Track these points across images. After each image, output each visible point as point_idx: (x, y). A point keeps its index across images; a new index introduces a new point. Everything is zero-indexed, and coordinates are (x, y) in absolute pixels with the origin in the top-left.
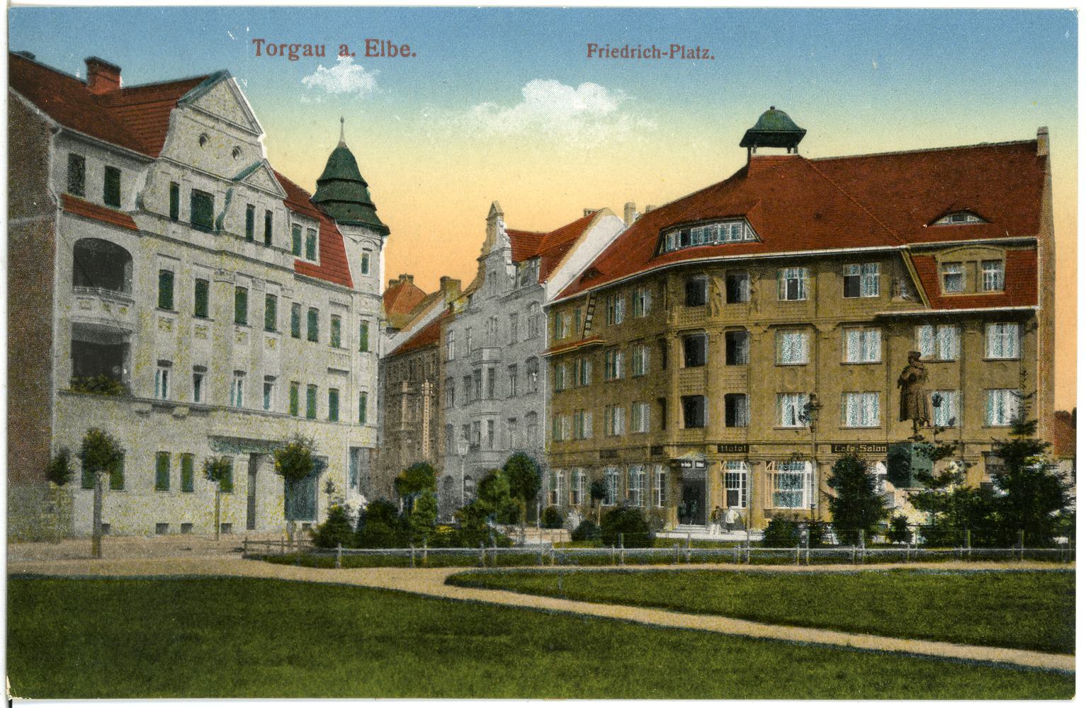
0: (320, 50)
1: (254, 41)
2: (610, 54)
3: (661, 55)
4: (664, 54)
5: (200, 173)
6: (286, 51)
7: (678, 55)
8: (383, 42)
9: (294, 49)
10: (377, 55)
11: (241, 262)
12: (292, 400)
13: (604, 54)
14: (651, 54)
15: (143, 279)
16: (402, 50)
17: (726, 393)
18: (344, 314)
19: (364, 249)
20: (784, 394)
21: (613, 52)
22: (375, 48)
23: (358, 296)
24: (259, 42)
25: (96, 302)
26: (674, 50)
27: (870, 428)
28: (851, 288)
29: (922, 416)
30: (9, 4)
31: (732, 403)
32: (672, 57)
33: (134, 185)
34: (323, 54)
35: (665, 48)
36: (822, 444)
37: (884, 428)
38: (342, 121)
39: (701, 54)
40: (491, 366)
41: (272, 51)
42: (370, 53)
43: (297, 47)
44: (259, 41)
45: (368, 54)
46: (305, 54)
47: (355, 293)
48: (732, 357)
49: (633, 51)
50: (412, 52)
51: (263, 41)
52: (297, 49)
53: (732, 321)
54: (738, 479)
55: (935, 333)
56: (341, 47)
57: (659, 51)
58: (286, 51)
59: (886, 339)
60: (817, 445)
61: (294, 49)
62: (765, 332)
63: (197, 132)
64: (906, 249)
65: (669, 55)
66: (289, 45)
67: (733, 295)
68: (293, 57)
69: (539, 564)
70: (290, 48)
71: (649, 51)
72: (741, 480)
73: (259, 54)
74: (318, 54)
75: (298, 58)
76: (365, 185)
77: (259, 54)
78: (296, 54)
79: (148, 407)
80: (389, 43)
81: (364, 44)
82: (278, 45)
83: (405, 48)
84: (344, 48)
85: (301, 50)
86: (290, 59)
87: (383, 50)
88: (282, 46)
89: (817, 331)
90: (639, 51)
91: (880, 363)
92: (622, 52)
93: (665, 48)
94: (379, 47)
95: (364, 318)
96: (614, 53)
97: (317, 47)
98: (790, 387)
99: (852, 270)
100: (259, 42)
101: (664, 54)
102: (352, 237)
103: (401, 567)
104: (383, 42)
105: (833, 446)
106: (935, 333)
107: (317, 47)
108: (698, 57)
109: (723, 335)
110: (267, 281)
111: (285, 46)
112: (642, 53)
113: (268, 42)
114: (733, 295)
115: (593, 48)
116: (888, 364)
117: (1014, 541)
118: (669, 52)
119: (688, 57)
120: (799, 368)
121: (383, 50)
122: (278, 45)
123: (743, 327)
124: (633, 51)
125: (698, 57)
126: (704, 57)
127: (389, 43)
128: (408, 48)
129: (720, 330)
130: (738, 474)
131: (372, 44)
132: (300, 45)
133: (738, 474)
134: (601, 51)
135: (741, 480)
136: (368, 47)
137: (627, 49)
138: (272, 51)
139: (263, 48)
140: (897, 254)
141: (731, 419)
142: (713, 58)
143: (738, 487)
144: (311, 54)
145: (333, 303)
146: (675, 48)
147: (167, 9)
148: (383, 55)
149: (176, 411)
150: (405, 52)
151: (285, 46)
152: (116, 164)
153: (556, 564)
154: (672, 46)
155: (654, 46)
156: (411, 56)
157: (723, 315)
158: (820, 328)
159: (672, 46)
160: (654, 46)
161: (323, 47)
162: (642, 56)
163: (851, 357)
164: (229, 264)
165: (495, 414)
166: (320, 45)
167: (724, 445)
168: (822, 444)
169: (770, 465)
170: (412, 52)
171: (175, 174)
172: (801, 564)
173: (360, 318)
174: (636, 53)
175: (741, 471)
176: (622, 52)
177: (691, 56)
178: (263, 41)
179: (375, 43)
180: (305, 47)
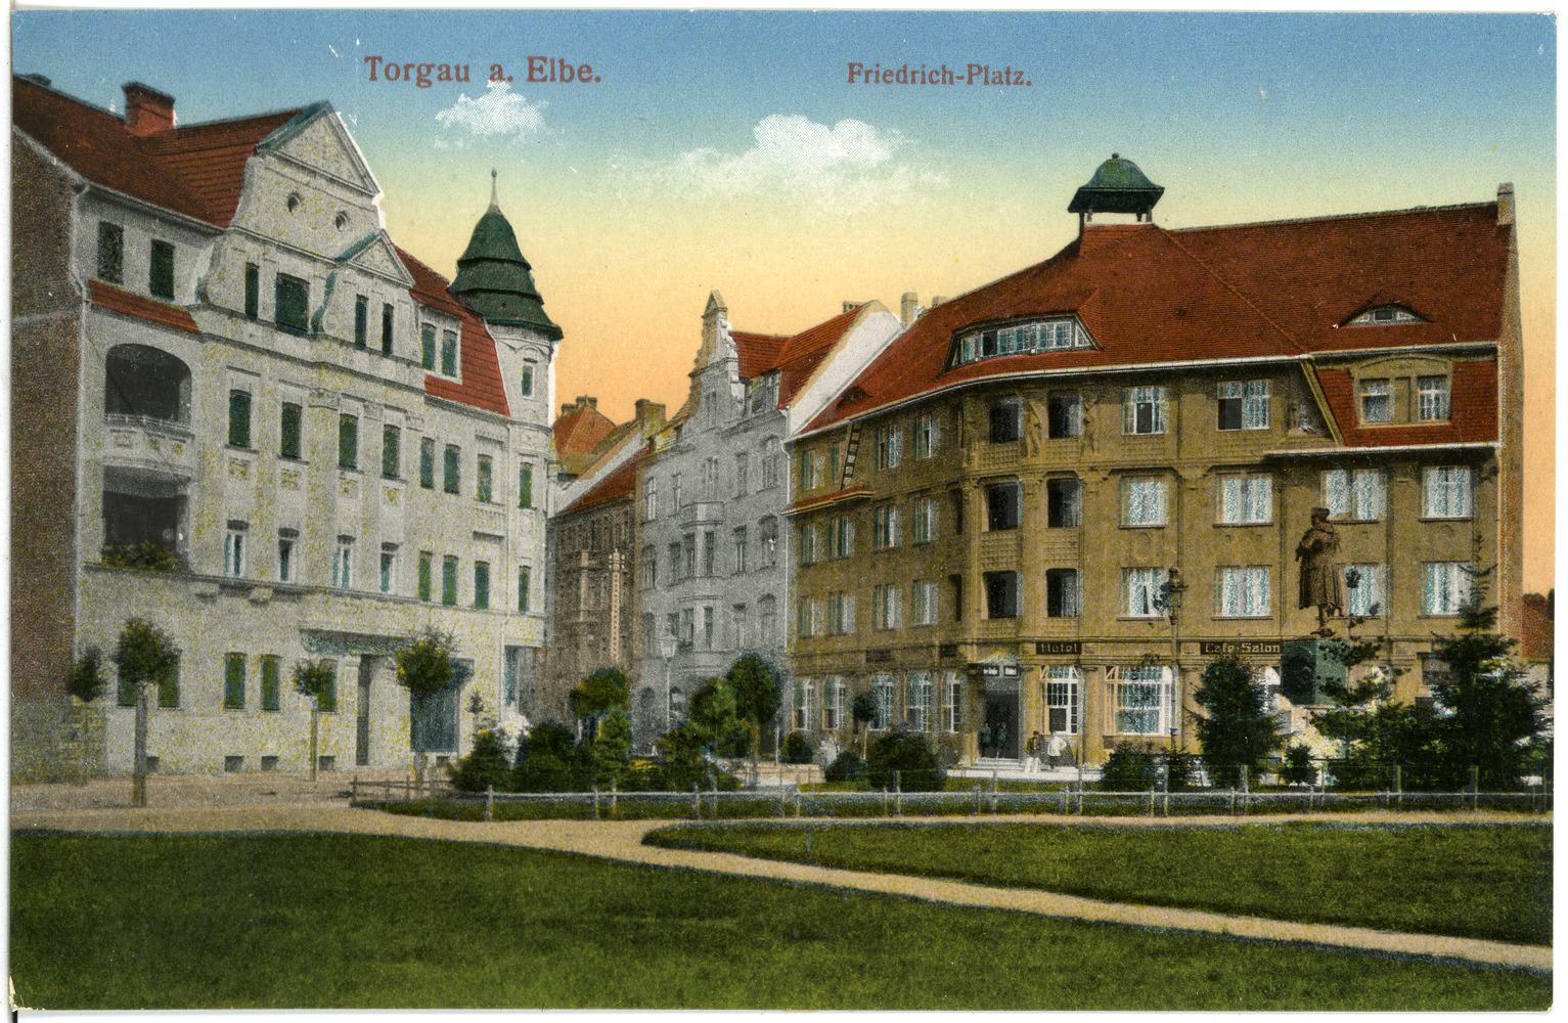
0: (462, 72)
1: (367, 59)
2: (880, 79)
3: (955, 80)
4: (959, 78)
5: (289, 250)
6: (413, 73)
7: (978, 80)
8: (552, 61)
9: (424, 71)
10: (544, 80)
11: (348, 379)
12: (422, 578)
13: (872, 77)
14: (940, 77)
15: (206, 404)
16: (580, 72)
17: (1048, 567)
18: (496, 454)
19: (525, 360)
20: (1131, 570)
21: (885, 75)
22: (541, 69)
23: (517, 428)
24: (373, 60)
25: (139, 436)
26: (973, 72)
27: (1256, 619)
28: (1229, 416)
30: (13, 6)
31: (1057, 582)
32: (970, 82)
33: (193, 267)
34: (467, 79)
35: (960, 70)
36: (1187, 641)
37: (1276, 618)
38: (494, 175)
39: (1012, 78)
40: (709, 528)
41: (392, 74)
42: (535, 77)
43: (429, 68)
44: (374, 59)
45: (531, 79)
46: (440, 78)
47: (513, 423)
48: (1057, 516)
49: (913, 73)
50: (594, 75)
51: (380, 59)
52: (429, 71)
53: (1057, 464)
54: (1066, 692)
55: (1350, 481)
56: (492, 68)
57: (951, 74)
58: (413, 73)
59: (1279, 489)
60: (1179, 643)
61: (424, 71)
62: (1105, 479)
63: (285, 191)
64: (1309, 360)
65: (966, 80)
66: (417, 65)
67: (1058, 427)
68: (423, 82)
69: (778, 815)
70: (419, 70)
71: (937, 73)
72: (1070, 694)
73: (373, 77)
74: (459, 79)
75: (430, 83)
76: (527, 267)
77: (373, 77)
78: (428, 78)
79: (214, 589)
80: (561, 61)
81: (526, 64)
82: (401, 64)
83: (585, 69)
84: (496, 69)
85: (435, 72)
86: (418, 85)
87: (553, 72)
88: (408, 67)
89: (1179, 479)
90: (923, 73)
91: (1271, 525)
92: (898, 75)
93: (960, 70)
94: (547, 68)
95: (526, 459)
96: (886, 77)
97: (458, 68)
98: (1141, 560)
99: (1230, 390)
100: (373, 60)
101: (959, 78)
102: (509, 342)
103: (578, 819)
104: (552, 61)
105: (1203, 644)
106: (1350, 481)
107: (458, 68)
108: (1008, 83)
109: (1044, 485)
110: (386, 406)
111: (412, 66)
112: (927, 77)
113: (387, 60)
114: (1058, 427)
115: (856, 69)
116: (1283, 527)
118: (966, 75)
119: (993, 82)
120: (1154, 532)
121: (553, 72)
122: (401, 64)
123: (1073, 472)
124: (913, 73)
125: (1008, 83)
126: (1016, 83)
127: (561, 61)
128: (589, 70)
129: (1040, 477)
130: (1066, 685)
131: (537, 63)
132: (433, 66)
133: (1066, 685)
134: (867, 73)
135: (1070, 694)
136: (531, 69)
137: (905, 71)
138: (392, 74)
139: (380, 69)
140: (1295, 367)
141: (1055, 606)
142: (1029, 83)
143: (1066, 703)
144: (449, 78)
145: (481, 438)
146: (975, 70)
147: (241, 13)
148: (553, 79)
149: (255, 594)
150: (585, 76)
151: (412, 66)
152: (168, 237)
153: (803, 815)
154: (970, 66)
155: (944, 67)
156: (593, 81)
157: (1044, 455)
158: (1185, 473)
159: (970, 66)
160: (944, 67)
161: (466, 68)
162: (927, 80)
163: (1229, 515)
164: (331, 381)
165: (714, 598)
166: (462, 65)
167: (1046, 643)
168: (1187, 641)
169: (1111, 672)
170: (594, 75)
171: (253, 252)
173: (519, 459)
174: (918, 76)
175: (1070, 681)
176: (898, 75)
177: (998, 80)
178: (380, 59)
179: (541, 62)
180: (440, 68)
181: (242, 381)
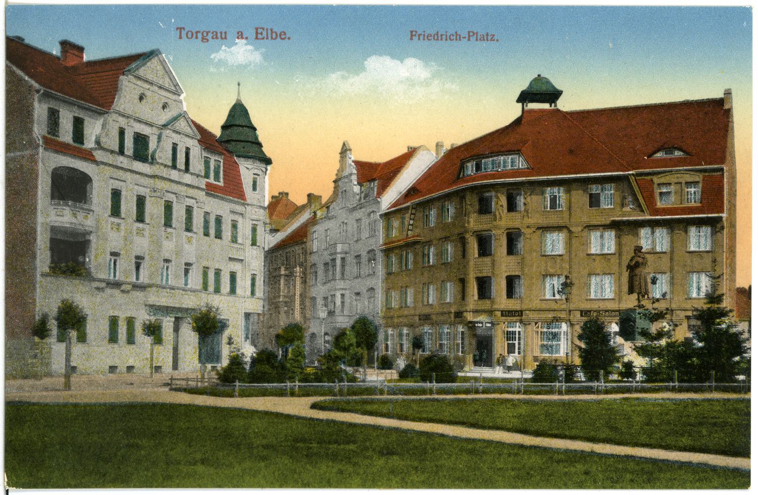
0: (223, 35)
1: (177, 29)
2: (426, 38)
3: (462, 39)
4: (463, 38)
5: (140, 121)
6: (200, 35)
7: (473, 39)
8: (267, 29)
9: (205, 34)
10: (263, 39)
11: (168, 183)
13: (422, 37)
14: (455, 37)
15: (100, 195)
16: (280, 35)
17: (507, 274)
18: (240, 220)
19: (254, 174)
20: (547, 276)
21: (428, 36)
22: (261, 34)
23: (250, 207)
24: (181, 29)
25: (67, 211)
26: (470, 35)
27: (607, 299)
28: (594, 201)
29: (643, 291)
30: (6, 3)
31: (511, 282)
32: (469, 40)
33: (93, 129)
34: (226, 38)
35: (464, 34)
36: (574, 310)
37: (617, 299)
38: (239, 85)
39: (489, 38)
40: (343, 256)
41: (190, 36)
42: (259, 37)
43: (207, 33)
44: (181, 29)
45: (257, 38)
46: (213, 38)
47: (248, 205)
48: (511, 250)
49: (442, 35)
50: (287, 36)
51: (184, 29)
52: (207, 35)
53: (511, 224)
54: (515, 335)
55: (653, 233)
56: (238, 33)
57: (460, 36)
58: (200, 35)
59: (618, 237)
60: (570, 311)
61: (205, 34)
62: (534, 232)
63: (138, 92)
64: (633, 174)
65: (467, 39)
66: (202, 31)
67: (512, 207)
68: (205, 40)
69: (376, 394)
70: (203, 34)
71: (453, 36)
72: (517, 336)
73: (180, 37)
74: (222, 38)
75: (208, 40)
76: (255, 129)
77: (180, 37)
78: (207, 38)
79: (103, 285)
80: (271, 30)
81: (254, 31)
82: (194, 31)
83: (283, 33)
84: (240, 33)
85: (210, 35)
86: (202, 41)
87: (267, 35)
88: (197, 32)
89: (570, 232)
90: (446, 35)
91: (614, 254)
92: (434, 36)
93: (464, 34)
94: (265, 33)
95: (254, 222)
96: (428, 37)
97: (221, 33)
98: (552, 271)
99: (595, 189)
100: (181, 29)
101: (463, 38)
102: (246, 166)
104: (267, 29)
105: (581, 312)
106: (653, 233)
107: (221, 33)
108: (487, 40)
109: (505, 235)
110: (187, 196)
111: (199, 32)
112: (448, 37)
113: (187, 29)
114: (512, 207)
115: (414, 33)
117: (708, 378)
118: (467, 36)
119: (480, 40)
120: (558, 257)
121: (267, 35)
122: (194, 31)
123: (519, 228)
124: (442, 35)
125: (487, 40)
126: (491, 40)
127: (271, 30)
128: (285, 34)
129: (503, 231)
130: (515, 332)
131: (260, 31)
132: (209, 32)
133: (515, 332)
134: (419, 35)
135: (517, 336)
136: (257, 33)
137: (437, 35)
138: (190, 36)
139: (184, 33)
141: (510, 293)
142: (497, 40)
143: (515, 340)
144: (217, 38)
145: (233, 212)
146: (471, 34)
148: (267, 38)
149: (123, 287)
150: (283, 37)
151: (199, 32)
152: (81, 115)
153: (388, 394)
154: (469, 32)
155: (456, 32)
156: (287, 39)
157: (505, 220)
158: (573, 229)
159: (469, 32)
160: (456, 32)
161: (225, 33)
162: (448, 39)
163: (594, 249)
164: (160, 184)
165: (345, 289)
166: (223, 32)
167: (506, 311)
168: (574, 310)
169: (537, 325)
170: (287, 36)
171: (122, 122)
172: (559, 394)
173: (251, 222)
174: (444, 37)
175: (517, 329)
176: (434, 36)
177: (483, 39)
178: (184, 29)
179: (262, 30)
180: (213, 33)
181: (117, 185)
